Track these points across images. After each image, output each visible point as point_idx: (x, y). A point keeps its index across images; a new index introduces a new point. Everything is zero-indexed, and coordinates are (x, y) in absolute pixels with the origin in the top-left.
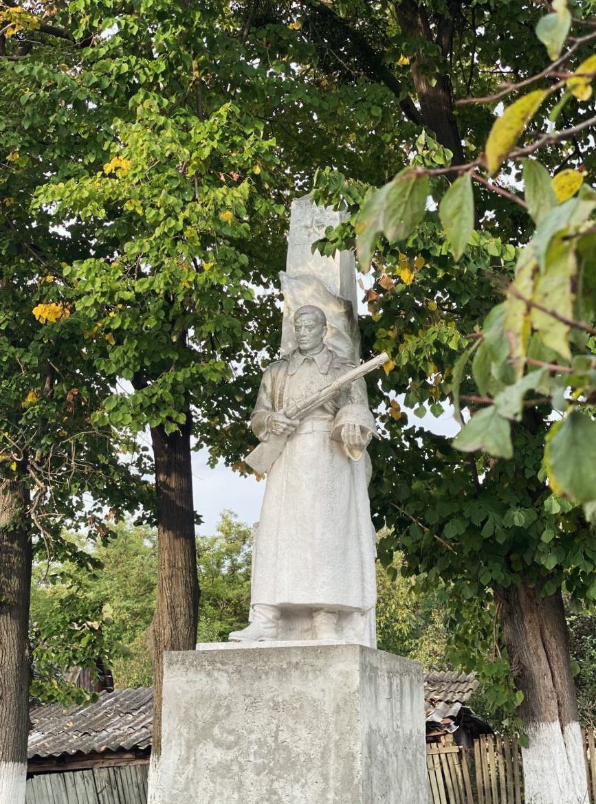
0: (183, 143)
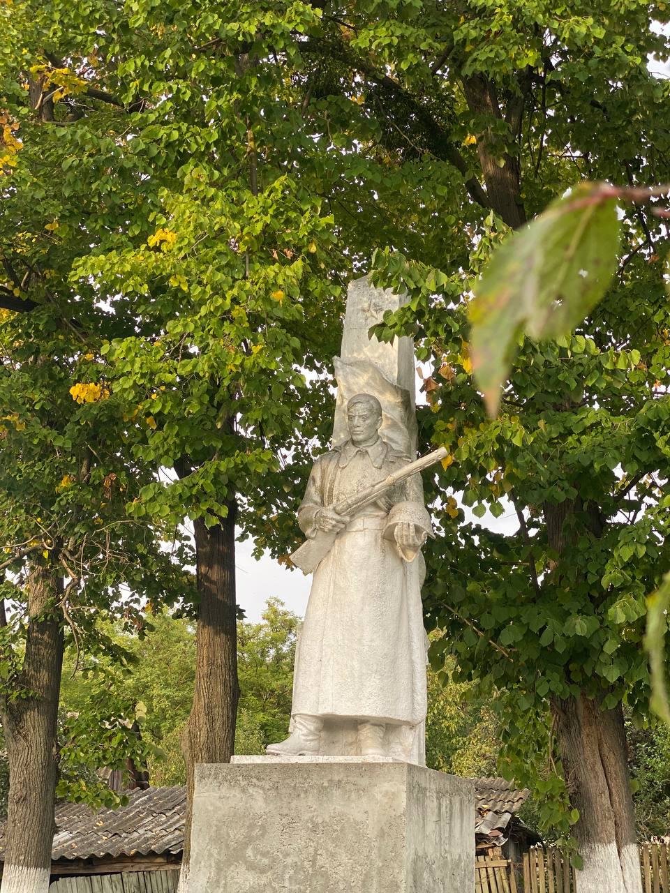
0: (234, 217)
